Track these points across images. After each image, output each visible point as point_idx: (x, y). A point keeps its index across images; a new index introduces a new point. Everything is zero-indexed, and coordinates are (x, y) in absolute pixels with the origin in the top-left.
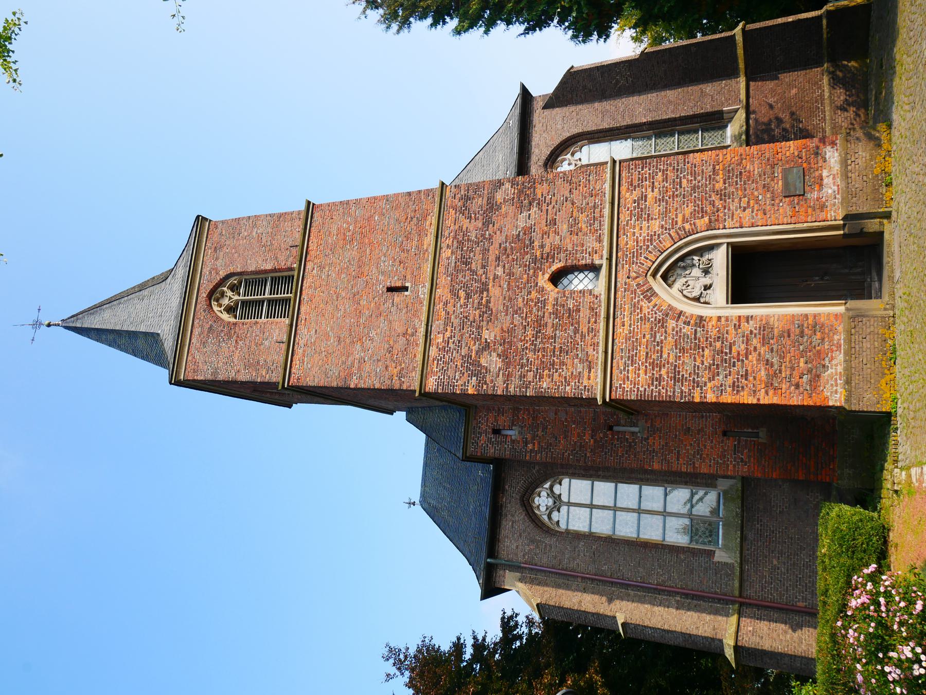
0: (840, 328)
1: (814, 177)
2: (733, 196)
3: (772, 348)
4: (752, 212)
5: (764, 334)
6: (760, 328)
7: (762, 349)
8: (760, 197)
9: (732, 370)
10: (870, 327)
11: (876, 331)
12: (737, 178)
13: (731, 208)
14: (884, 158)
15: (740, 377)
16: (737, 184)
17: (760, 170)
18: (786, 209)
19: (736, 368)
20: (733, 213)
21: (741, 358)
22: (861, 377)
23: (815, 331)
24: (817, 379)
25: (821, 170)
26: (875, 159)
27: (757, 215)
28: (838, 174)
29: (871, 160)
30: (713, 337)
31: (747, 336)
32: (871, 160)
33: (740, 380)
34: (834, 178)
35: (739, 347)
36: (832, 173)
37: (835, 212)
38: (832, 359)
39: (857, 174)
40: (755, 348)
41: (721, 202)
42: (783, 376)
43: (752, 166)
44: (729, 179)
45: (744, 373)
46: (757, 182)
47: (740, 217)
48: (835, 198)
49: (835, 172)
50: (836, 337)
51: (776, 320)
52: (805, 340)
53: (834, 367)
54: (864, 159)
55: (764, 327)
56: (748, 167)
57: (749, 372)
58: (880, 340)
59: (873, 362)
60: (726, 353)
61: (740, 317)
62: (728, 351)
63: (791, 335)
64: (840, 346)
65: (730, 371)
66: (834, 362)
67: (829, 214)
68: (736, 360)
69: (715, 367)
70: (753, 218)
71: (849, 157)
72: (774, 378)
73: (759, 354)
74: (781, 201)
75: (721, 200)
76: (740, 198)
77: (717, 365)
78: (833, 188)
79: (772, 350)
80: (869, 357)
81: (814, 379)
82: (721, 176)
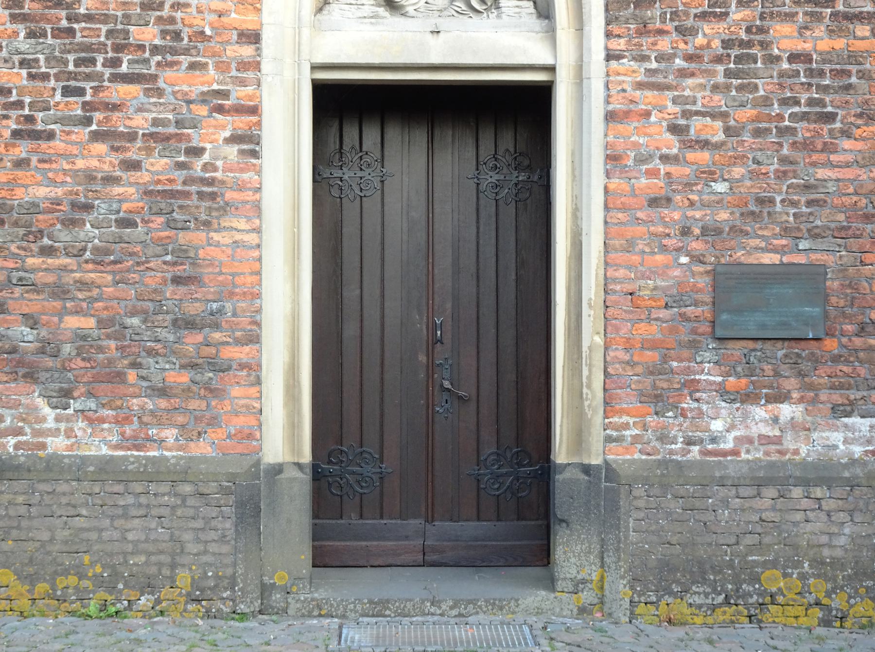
0: (203, 448)
1: (777, 374)
2: (740, 88)
3: (134, 225)
4: (665, 158)
5: (187, 195)
6: (211, 182)
7: (132, 190)
8: (721, 187)
9: (52, 83)
10: (198, 540)
11: (186, 560)
12: (811, 102)
13: (690, 81)
14: (818, 603)
15: (27, 112)
16: (784, 102)
17: (832, 188)
18: (663, 275)
19: (58, 97)
20: (668, 87)
21: (98, 116)
22: (23, 510)
23: (193, 366)
24: (22, 371)
25: (801, 400)
26: (818, 576)
27: (652, 173)
28: (781, 453)
29: (819, 563)
30: (179, 15)
31: (179, 137)
32: (819, 563)
33: (14, 114)
34: (765, 440)
35: (140, 110)
36: (789, 436)
37: (636, 439)
38: (91, 421)
39: (768, 515)
40: (134, 166)
41: (716, 43)
42: (30, 261)
43: (850, 157)
44: (810, 73)
45: (40, 127)
46: (781, 175)
47: (647, 114)
48: (689, 442)
49: (789, 443)
50: (170, 434)
51: (238, 237)
52: (163, 334)
53: (63, 426)
54: (824, 539)
55: (213, 196)
56: (847, 144)
57: (44, 145)
58: (153, 570)
59: (75, 548)
60: (115, 63)
61: (254, 110)
62: (124, 68)
63: (182, 289)
64: (137, 448)
65: (45, 77)
66: (80, 424)
67: (631, 421)
68: (88, 98)
69: (64, 23)
70: (641, 160)
71: (839, 492)
72: (21, 231)
73: (110, 180)
74: (698, 259)
75: (727, 44)
76: (724, 116)
77: (71, 32)
78: (731, 437)
79: (126, 223)
80: (94, 536)
81: (20, 363)
82: (825, 45)
